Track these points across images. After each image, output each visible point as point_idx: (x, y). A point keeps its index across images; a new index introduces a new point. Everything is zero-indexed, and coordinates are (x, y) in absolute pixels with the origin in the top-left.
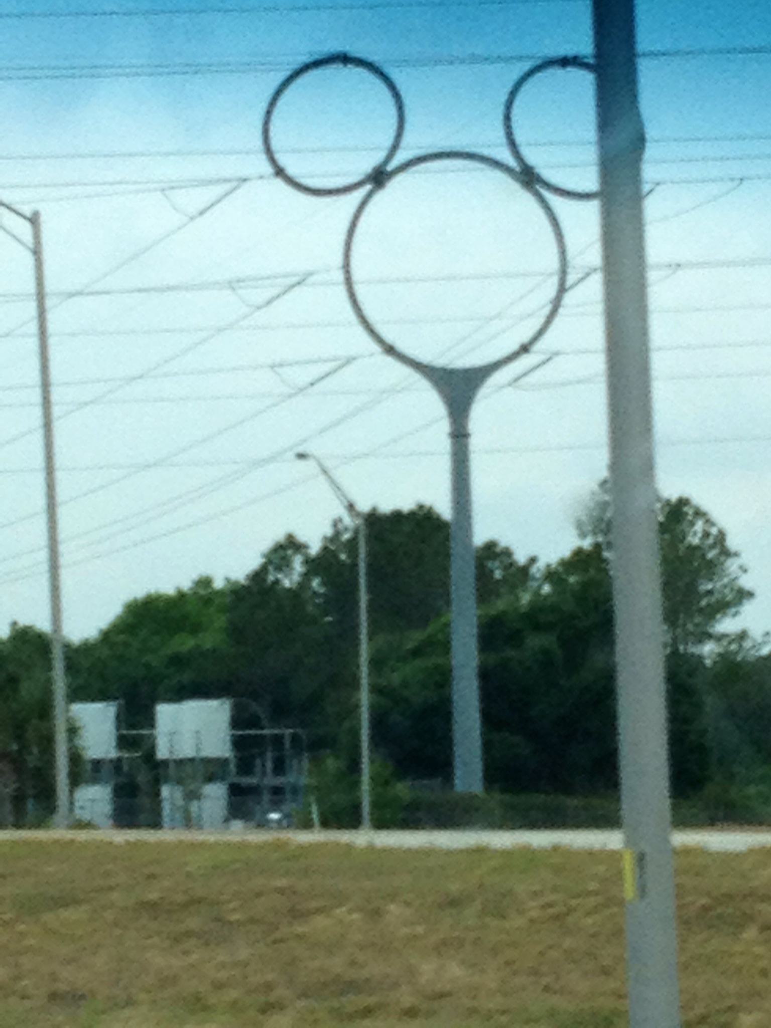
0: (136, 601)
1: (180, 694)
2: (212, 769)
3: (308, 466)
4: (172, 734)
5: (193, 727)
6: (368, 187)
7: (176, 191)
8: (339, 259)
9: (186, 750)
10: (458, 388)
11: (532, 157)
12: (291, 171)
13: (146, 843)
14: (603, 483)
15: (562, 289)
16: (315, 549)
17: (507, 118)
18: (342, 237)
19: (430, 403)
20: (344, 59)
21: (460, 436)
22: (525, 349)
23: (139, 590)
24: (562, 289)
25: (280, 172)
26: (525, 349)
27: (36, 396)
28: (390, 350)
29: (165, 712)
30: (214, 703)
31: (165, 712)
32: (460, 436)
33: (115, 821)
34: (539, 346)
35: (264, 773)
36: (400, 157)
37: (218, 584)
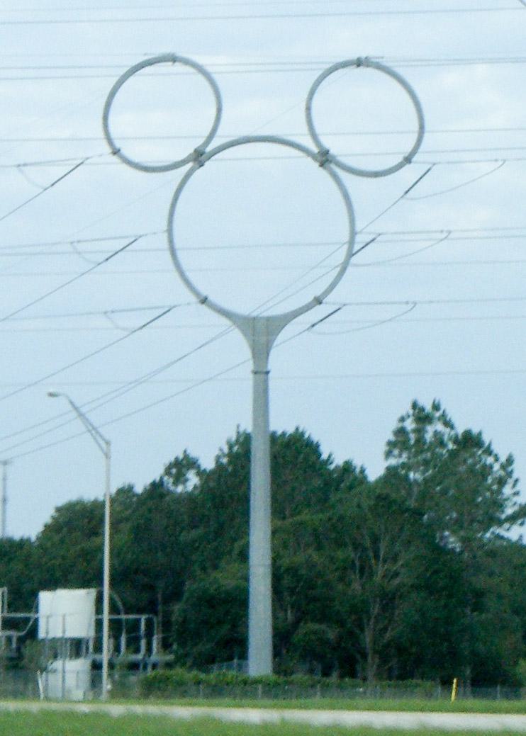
1: (53, 583)
2: (77, 647)
3: (62, 404)
4: (48, 617)
6: (190, 165)
7: (29, 167)
8: (165, 226)
10: (261, 333)
11: (327, 143)
13: (208, 706)
15: (351, 254)
16: (208, 464)
17: (105, 118)
18: (168, 206)
19: (238, 347)
21: (261, 374)
22: (318, 301)
23: (62, 502)
25: (116, 152)
26: (318, 301)
31: (46, 599)
32: (261, 374)
34: (330, 298)
35: (149, 650)
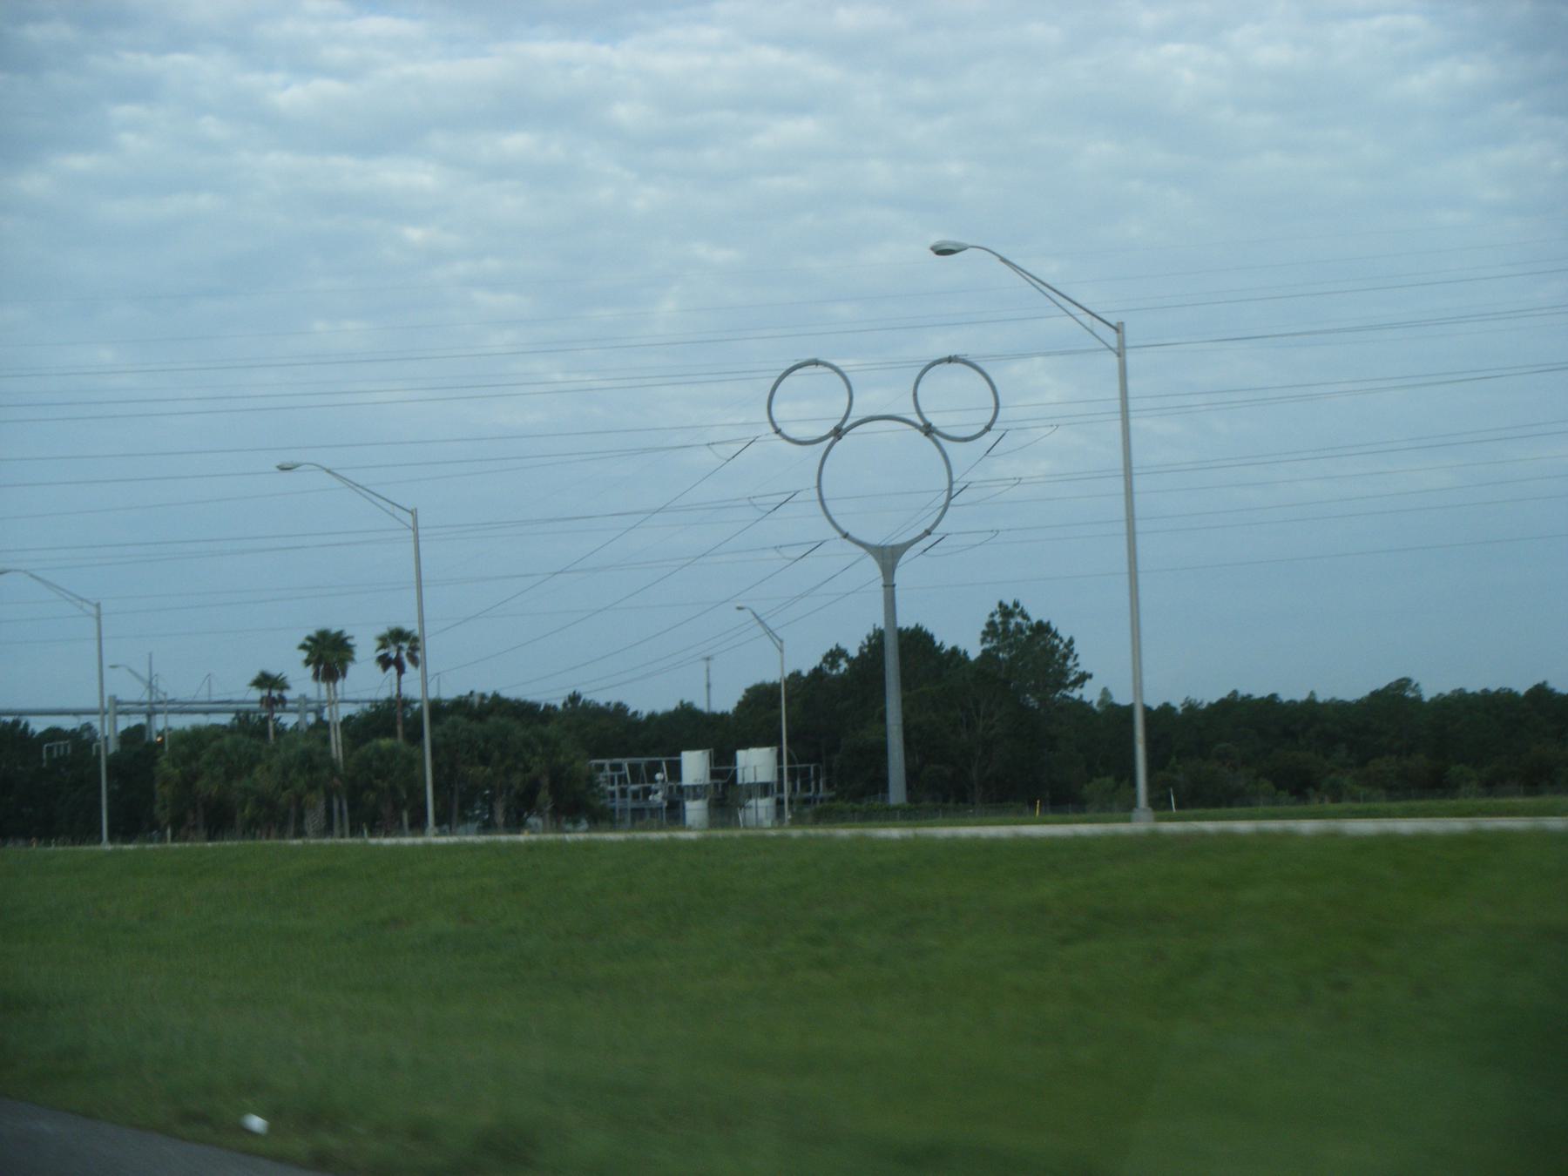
0: (620, 709)
1: (746, 744)
2: (765, 789)
3: (747, 615)
5: (755, 763)
8: (815, 483)
9: (750, 779)
10: (888, 557)
11: (930, 418)
12: (785, 431)
14: (483, 696)
15: (950, 498)
16: (854, 653)
19: (871, 569)
20: (816, 363)
21: (889, 586)
24: (950, 498)
26: (928, 532)
27: (1122, 528)
28: (846, 536)
29: (741, 755)
30: (767, 750)
31: (741, 755)
32: (889, 586)
33: (1084, 703)
34: (939, 529)
36: (849, 422)
37: (805, 673)
